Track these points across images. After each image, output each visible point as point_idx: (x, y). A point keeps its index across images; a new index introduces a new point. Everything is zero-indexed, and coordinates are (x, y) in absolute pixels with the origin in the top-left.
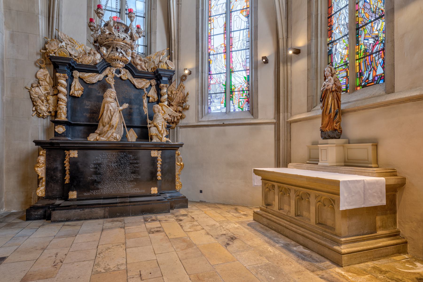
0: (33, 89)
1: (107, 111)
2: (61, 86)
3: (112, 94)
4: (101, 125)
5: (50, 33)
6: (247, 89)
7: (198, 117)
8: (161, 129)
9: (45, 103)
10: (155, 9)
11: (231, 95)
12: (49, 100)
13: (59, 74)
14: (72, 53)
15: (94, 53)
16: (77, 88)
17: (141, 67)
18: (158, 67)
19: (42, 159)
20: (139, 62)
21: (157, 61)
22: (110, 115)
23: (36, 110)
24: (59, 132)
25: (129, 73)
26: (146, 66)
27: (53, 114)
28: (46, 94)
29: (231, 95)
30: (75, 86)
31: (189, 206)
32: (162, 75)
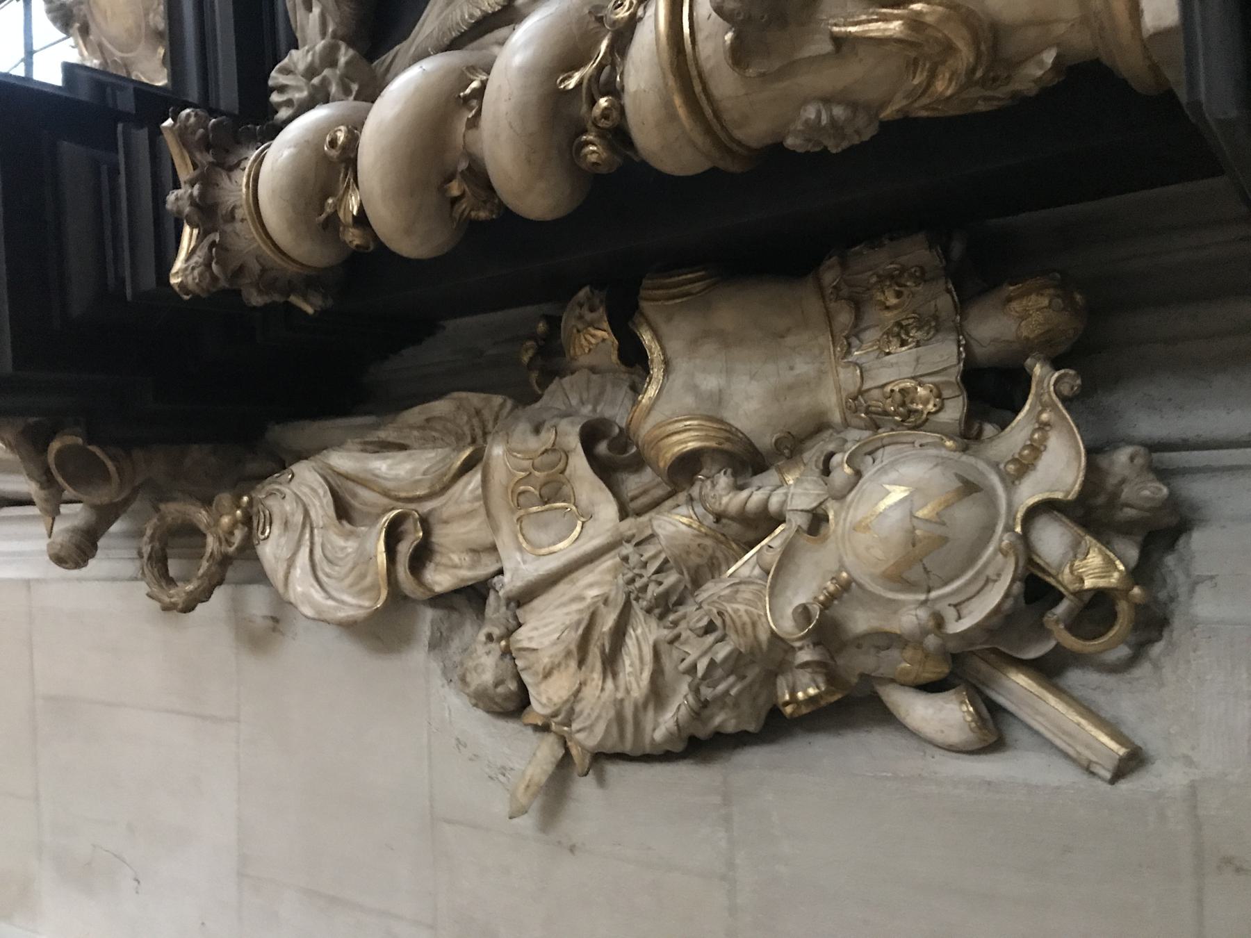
0: (546, 696)
2: (348, 156)
23: (960, 668)
27: (997, 327)
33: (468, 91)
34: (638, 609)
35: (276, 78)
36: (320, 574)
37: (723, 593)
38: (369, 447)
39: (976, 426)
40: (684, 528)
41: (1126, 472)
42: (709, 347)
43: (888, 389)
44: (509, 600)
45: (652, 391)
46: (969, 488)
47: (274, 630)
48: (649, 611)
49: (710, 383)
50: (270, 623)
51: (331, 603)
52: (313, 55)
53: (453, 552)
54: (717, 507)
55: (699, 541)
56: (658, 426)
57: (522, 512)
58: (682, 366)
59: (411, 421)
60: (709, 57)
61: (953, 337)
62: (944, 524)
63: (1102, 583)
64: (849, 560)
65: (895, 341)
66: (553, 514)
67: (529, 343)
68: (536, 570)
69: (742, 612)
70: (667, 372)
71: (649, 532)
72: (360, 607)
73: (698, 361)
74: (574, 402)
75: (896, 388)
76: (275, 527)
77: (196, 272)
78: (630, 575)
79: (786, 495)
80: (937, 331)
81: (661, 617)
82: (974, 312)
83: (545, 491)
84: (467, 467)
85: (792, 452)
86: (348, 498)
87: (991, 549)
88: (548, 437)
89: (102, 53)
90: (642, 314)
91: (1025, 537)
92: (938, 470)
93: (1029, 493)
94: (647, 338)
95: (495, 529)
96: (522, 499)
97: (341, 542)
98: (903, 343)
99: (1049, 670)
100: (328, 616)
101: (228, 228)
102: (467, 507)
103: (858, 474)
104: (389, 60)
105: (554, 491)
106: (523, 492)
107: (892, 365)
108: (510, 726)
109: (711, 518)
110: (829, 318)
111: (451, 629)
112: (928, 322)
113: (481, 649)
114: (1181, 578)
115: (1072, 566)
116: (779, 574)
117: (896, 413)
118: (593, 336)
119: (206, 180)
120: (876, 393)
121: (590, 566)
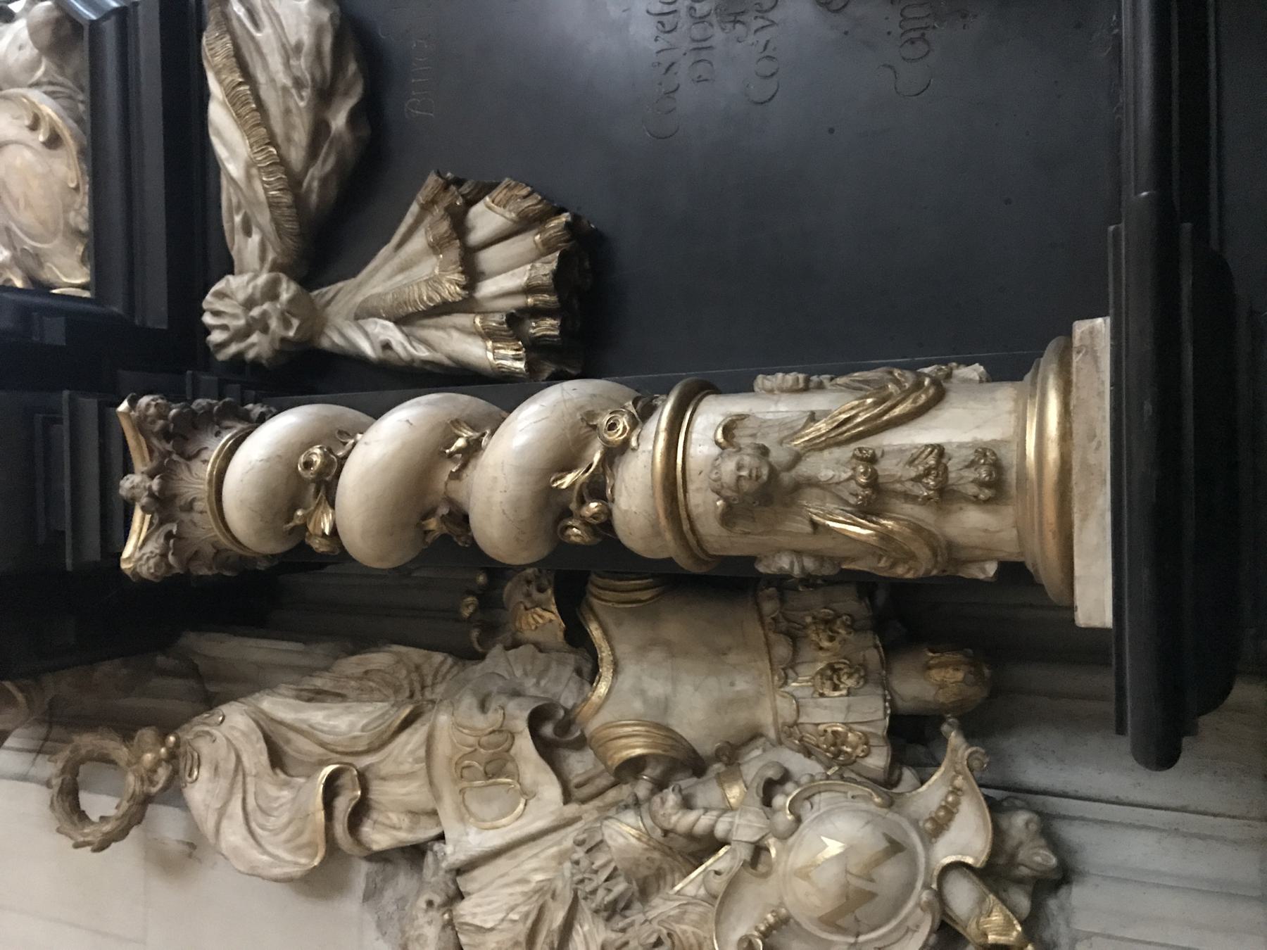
2: (326, 483)
9: (727, 806)
27: (932, 682)
28: (579, 764)
33: (453, 449)
34: (586, 908)
35: (209, 301)
36: (253, 825)
37: (672, 913)
38: (305, 694)
39: (897, 773)
40: (633, 841)
41: (1023, 836)
42: (656, 655)
43: (821, 728)
44: (449, 871)
45: (602, 688)
46: (895, 847)
47: (190, 856)
48: (596, 912)
49: (657, 688)
50: (186, 849)
51: (265, 858)
52: (255, 288)
53: (392, 811)
54: (667, 826)
55: (648, 854)
56: (607, 726)
57: (465, 784)
58: (631, 671)
59: (349, 672)
60: (697, 506)
61: (880, 691)
62: (872, 880)
63: (1002, 940)
64: (788, 900)
65: (828, 683)
66: (493, 789)
67: (470, 599)
68: (479, 845)
69: (689, 934)
70: (616, 672)
71: (598, 838)
72: (296, 864)
73: (645, 666)
74: (518, 673)
75: (829, 730)
76: (202, 769)
77: (152, 562)
78: (580, 877)
79: (731, 823)
80: (866, 682)
81: (608, 919)
82: (898, 667)
83: (490, 768)
84: (407, 723)
85: (729, 758)
86: (281, 743)
87: (911, 904)
88: (493, 718)
89: (9, 236)
90: (591, 609)
91: (940, 895)
92: (869, 828)
93: (944, 854)
94: (595, 631)
95: (437, 798)
96: (466, 772)
97: (272, 791)
98: (836, 688)
100: (265, 873)
101: (185, 516)
102: (406, 768)
103: (798, 820)
104: (331, 295)
105: (497, 766)
106: (469, 767)
107: (826, 708)
109: (659, 832)
110: (769, 646)
111: (385, 880)
112: (857, 671)
113: (422, 919)
114: (1063, 929)
115: (978, 923)
116: (722, 901)
117: (827, 750)
118: (541, 616)
119: (163, 470)
120: (810, 728)
121: (532, 844)
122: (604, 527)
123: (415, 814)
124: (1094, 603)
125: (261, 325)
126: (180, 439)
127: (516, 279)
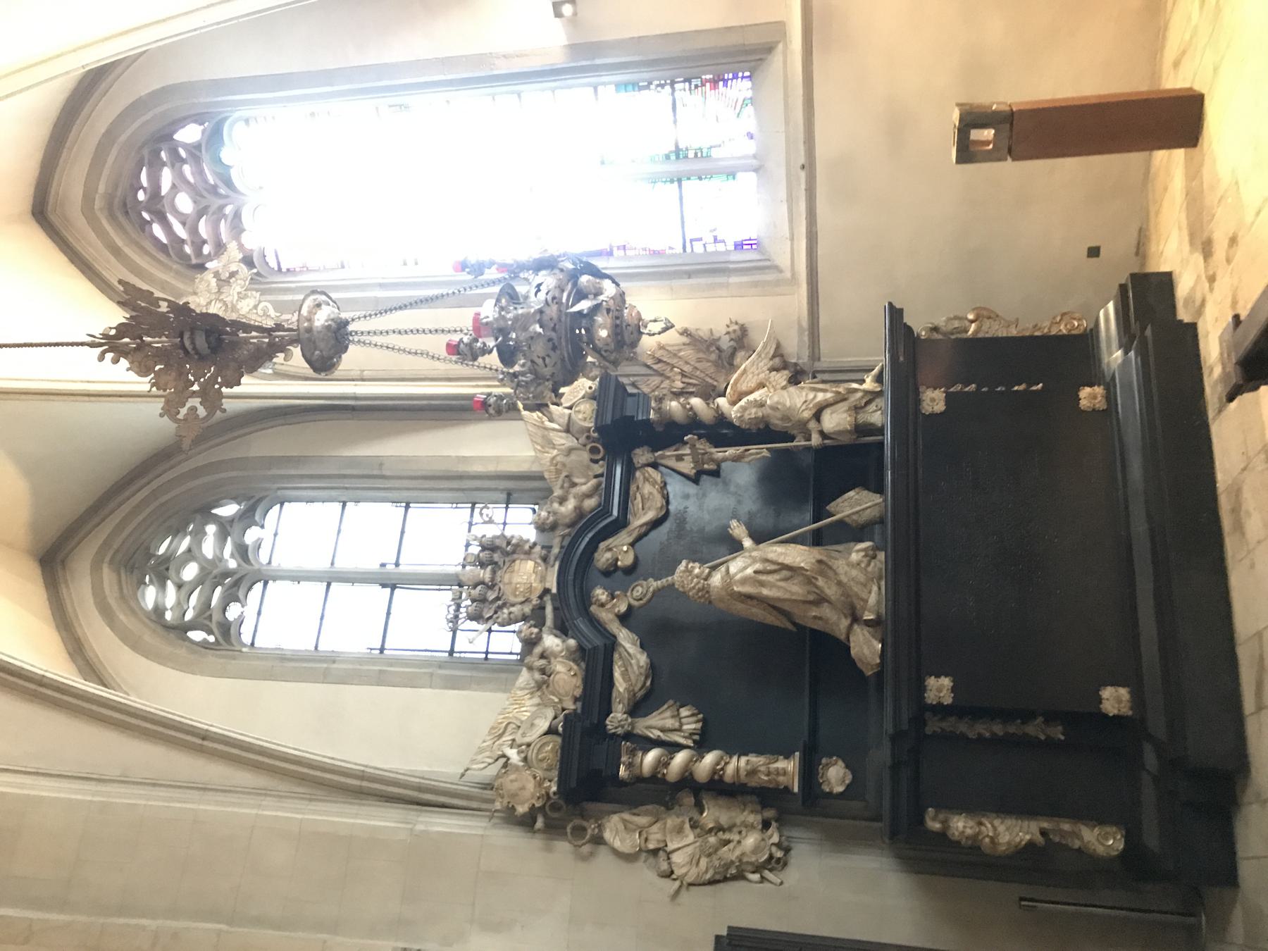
0: (678, 872)
1: (762, 584)
2: (667, 765)
3: (697, 571)
4: (814, 612)
5: (475, 805)
6: (668, 88)
7: (777, 283)
8: (829, 395)
10: (380, 462)
11: (691, 154)
12: (717, 822)
13: (622, 768)
14: (543, 725)
15: (542, 656)
16: (670, 723)
17: (588, 496)
18: (588, 430)
19: (960, 825)
20: (571, 504)
21: (563, 441)
22: (777, 576)
23: (758, 869)
24: (847, 782)
25: (610, 540)
26: (583, 480)
27: (770, 813)
29: (691, 154)
30: (663, 730)
31: (1164, 268)
32: (617, 416)
93: (772, 841)
99: (771, 870)
108: (667, 880)
122: (721, 777)
123: (658, 841)
124: (796, 790)
125: (623, 727)
126: (632, 753)
127: (693, 726)
